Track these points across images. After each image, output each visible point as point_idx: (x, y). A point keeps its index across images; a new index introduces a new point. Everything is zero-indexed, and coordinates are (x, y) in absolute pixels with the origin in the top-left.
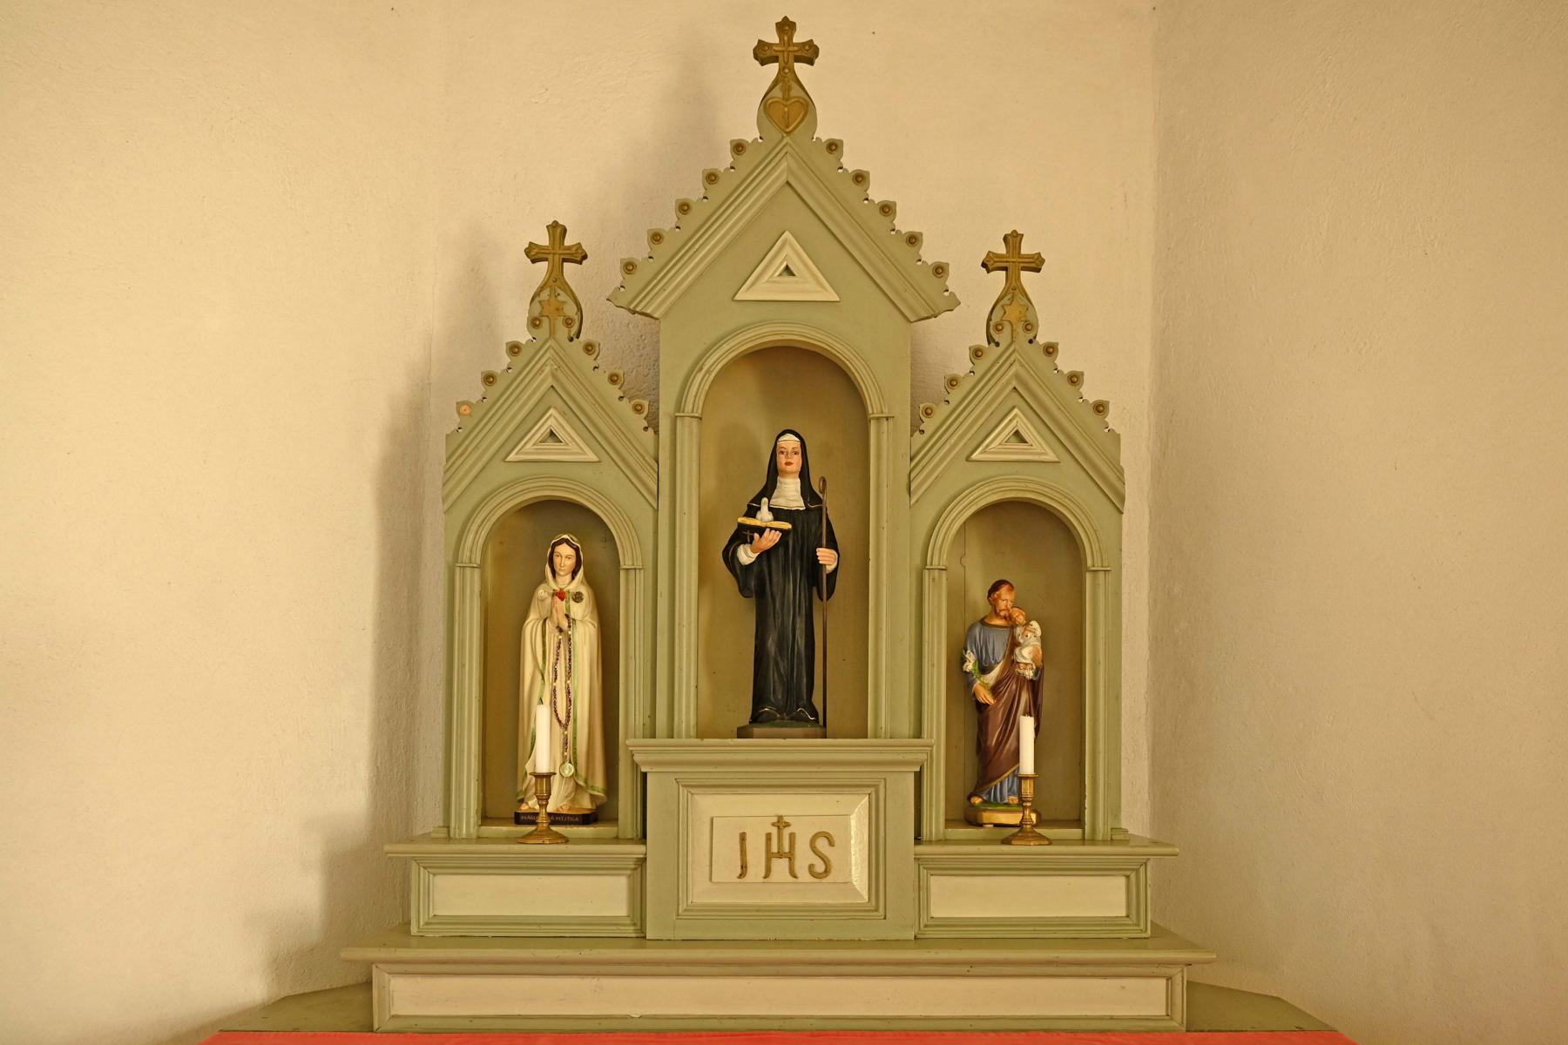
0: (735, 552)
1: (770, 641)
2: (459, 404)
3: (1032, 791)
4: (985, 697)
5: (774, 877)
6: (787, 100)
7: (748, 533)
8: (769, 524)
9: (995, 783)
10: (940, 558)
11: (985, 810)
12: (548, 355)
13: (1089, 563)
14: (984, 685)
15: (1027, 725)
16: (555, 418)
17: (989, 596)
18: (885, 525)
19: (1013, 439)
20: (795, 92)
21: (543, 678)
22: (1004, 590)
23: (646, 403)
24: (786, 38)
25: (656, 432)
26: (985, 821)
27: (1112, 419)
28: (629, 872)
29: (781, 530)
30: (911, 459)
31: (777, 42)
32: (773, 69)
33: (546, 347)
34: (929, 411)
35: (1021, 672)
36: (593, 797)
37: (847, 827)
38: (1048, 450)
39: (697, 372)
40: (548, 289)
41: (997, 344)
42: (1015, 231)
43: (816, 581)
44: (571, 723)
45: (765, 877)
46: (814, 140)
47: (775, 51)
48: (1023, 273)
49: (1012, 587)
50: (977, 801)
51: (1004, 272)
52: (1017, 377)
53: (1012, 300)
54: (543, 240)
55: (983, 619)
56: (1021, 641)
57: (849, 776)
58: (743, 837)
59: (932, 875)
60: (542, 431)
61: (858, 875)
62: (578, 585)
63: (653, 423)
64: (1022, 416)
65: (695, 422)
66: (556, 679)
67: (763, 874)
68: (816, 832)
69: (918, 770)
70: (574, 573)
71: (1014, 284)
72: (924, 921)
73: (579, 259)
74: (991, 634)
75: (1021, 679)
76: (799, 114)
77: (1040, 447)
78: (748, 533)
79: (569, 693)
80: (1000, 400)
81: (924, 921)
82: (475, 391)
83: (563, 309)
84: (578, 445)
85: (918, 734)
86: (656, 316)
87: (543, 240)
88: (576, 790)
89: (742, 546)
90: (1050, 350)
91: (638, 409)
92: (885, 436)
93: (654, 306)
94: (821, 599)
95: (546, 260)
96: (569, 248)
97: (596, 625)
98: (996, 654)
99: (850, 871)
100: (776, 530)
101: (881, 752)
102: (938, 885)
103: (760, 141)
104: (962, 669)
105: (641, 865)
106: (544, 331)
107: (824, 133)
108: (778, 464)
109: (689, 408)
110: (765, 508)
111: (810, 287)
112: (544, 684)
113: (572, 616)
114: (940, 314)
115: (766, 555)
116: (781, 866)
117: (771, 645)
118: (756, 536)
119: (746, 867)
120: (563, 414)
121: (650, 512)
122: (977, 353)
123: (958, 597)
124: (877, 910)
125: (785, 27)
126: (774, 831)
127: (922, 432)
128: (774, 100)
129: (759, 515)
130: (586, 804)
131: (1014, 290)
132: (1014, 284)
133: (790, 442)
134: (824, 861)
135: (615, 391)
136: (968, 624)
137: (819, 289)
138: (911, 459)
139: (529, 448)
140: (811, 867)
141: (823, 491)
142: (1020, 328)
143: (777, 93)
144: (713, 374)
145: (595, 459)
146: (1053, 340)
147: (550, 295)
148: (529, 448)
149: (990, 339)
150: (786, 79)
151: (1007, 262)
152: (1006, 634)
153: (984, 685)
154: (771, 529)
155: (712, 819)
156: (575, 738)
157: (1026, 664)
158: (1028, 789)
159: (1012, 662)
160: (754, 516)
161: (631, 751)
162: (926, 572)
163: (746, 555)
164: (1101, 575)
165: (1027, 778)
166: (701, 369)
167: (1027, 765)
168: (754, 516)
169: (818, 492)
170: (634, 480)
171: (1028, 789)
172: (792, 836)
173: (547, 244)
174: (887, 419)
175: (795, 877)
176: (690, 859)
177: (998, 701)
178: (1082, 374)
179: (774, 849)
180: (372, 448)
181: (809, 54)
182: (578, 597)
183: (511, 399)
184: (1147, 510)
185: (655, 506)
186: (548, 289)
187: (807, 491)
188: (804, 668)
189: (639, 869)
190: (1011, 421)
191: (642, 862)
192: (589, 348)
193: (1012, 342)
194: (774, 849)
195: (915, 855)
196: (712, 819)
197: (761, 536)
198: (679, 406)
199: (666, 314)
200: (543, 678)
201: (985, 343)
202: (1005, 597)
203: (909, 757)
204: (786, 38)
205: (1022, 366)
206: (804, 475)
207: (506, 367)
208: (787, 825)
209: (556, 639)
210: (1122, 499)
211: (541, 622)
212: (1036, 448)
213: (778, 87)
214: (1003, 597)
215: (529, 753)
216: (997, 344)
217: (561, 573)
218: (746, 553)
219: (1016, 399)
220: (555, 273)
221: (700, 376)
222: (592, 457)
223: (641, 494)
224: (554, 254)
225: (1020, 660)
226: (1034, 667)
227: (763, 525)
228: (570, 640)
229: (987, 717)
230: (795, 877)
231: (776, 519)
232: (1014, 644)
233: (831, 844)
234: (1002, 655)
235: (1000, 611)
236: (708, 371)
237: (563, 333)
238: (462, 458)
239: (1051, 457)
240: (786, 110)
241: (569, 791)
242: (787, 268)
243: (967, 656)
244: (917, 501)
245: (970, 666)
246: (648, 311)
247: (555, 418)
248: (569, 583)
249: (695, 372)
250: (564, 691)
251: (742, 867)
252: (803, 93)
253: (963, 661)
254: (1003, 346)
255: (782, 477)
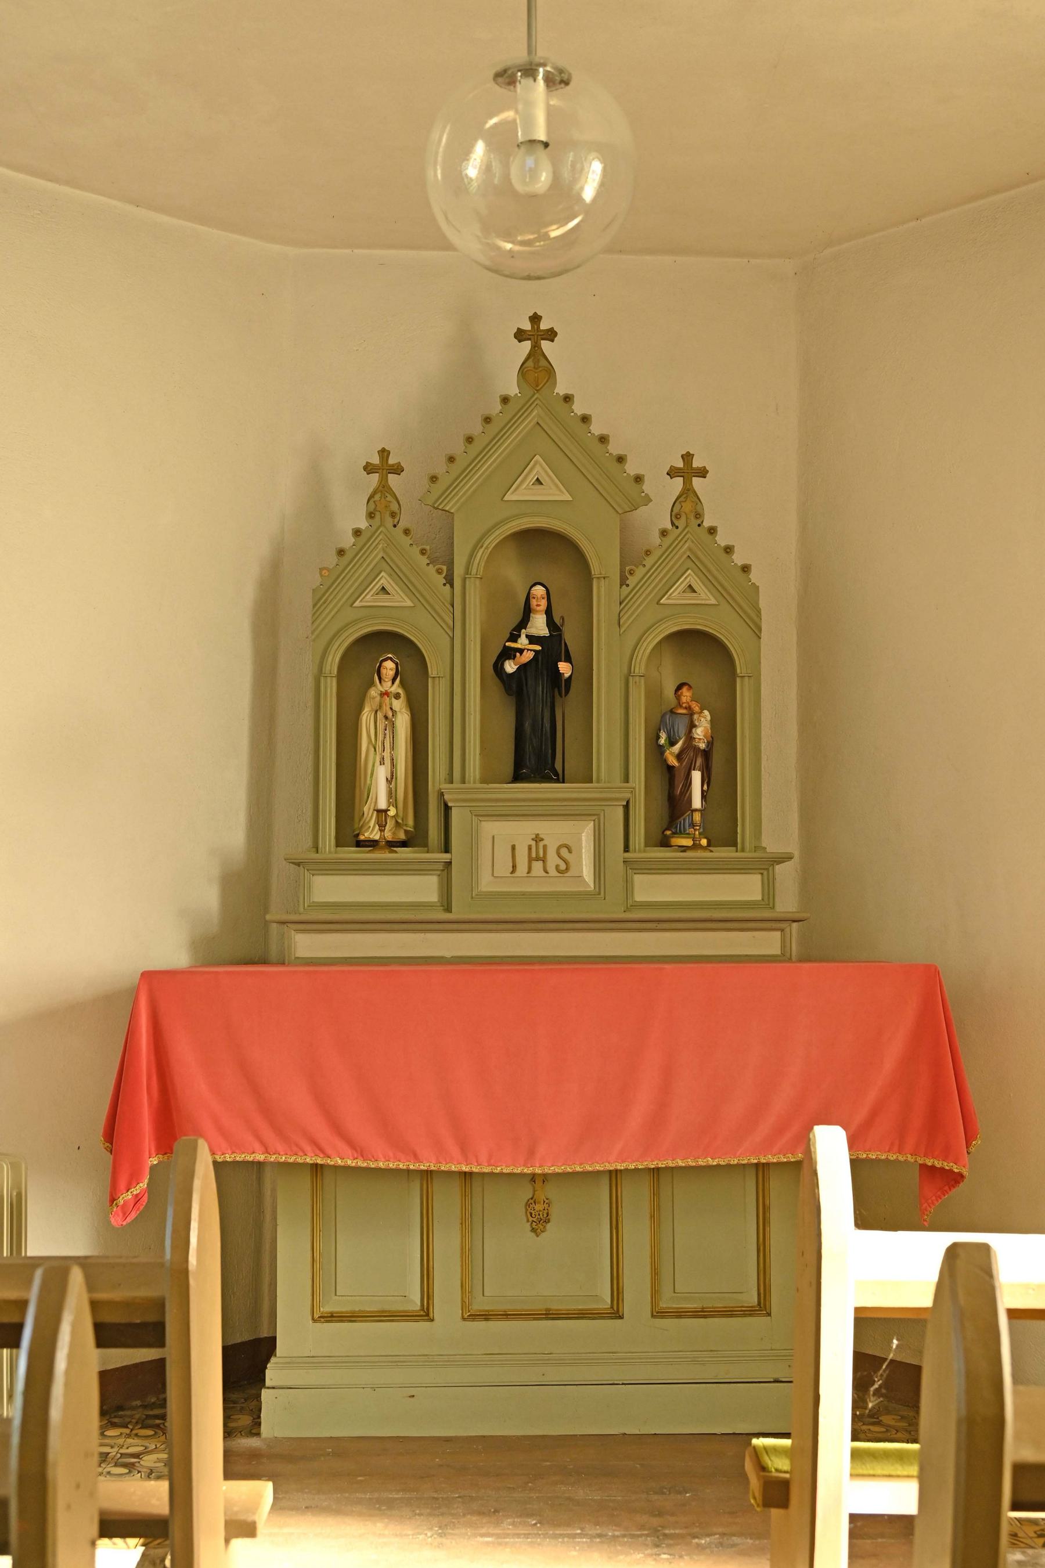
0: (503, 665)
1: (527, 724)
2: (321, 569)
3: (700, 819)
4: (673, 761)
5: (533, 873)
6: (537, 369)
7: (513, 652)
8: (527, 647)
9: (680, 820)
10: (639, 668)
11: (673, 837)
12: (381, 537)
13: (738, 671)
14: (672, 754)
15: (696, 776)
16: (386, 579)
17: (675, 694)
18: (603, 647)
19: (688, 590)
20: (543, 363)
21: (375, 750)
22: (685, 689)
23: (444, 568)
24: (536, 327)
25: (452, 586)
26: (673, 844)
27: (754, 576)
28: (439, 872)
29: (534, 651)
30: (620, 604)
31: (530, 329)
32: (527, 345)
33: (379, 532)
34: (632, 572)
35: (697, 744)
36: (406, 832)
37: (580, 840)
38: (711, 597)
39: (480, 548)
40: (380, 493)
41: (677, 527)
42: (688, 452)
43: (558, 685)
44: (394, 780)
45: (528, 873)
46: (555, 394)
47: (529, 335)
48: (694, 479)
49: (690, 687)
50: (668, 833)
51: (682, 478)
52: (690, 549)
53: (686, 498)
54: (376, 460)
55: (672, 709)
56: (697, 724)
57: (583, 808)
58: (513, 848)
59: (635, 874)
60: (377, 587)
61: (587, 873)
62: (396, 688)
63: (450, 581)
64: (693, 574)
65: (478, 582)
66: (384, 750)
67: (526, 871)
68: (560, 844)
69: (625, 803)
70: (394, 681)
71: (688, 487)
72: (630, 902)
73: (399, 473)
74: (677, 719)
75: (697, 749)
76: (545, 378)
77: (705, 595)
78: (513, 652)
79: (393, 760)
80: (673, 571)
81: (630, 902)
82: (332, 560)
83: (389, 506)
84: (402, 597)
85: (626, 779)
86: (452, 511)
87: (376, 460)
88: (396, 827)
89: (507, 662)
90: (712, 531)
91: (439, 572)
92: (603, 589)
93: (450, 505)
94: (561, 697)
95: (378, 473)
96: (393, 465)
97: (410, 715)
98: (679, 733)
99: (582, 869)
100: (531, 650)
101: (601, 792)
102: (639, 880)
103: (519, 395)
104: (657, 742)
105: (447, 868)
106: (377, 521)
107: (561, 389)
108: (531, 607)
109: (474, 571)
110: (523, 636)
111: (554, 492)
112: (376, 754)
113: (394, 708)
114: (638, 508)
115: (523, 668)
116: (538, 866)
117: (527, 725)
118: (518, 654)
119: (516, 866)
120: (390, 575)
121: (448, 640)
122: (664, 533)
123: (653, 694)
124: (762, 1307)
125: (535, 319)
126: (533, 843)
127: (628, 585)
128: (529, 369)
129: (519, 641)
130: (402, 836)
131: (688, 491)
132: (688, 487)
133: (539, 590)
134: (565, 862)
135: (407, 540)
136: (664, 712)
137: (558, 493)
138: (620, 604)
139: (369, 598)
140: (557, 867)
141: (562, 626)
142: (692, 517)
143: (530, 363)
144: (490, 549)
145: (412, 605)
146: (714, 525)
147: (381, 497)
148: (369, 598)
149: (673, 524)
150: (536, 352)
151: (683, 472)
152: (686, 720)
153: (672, 754)
154: (528, 650)
155: (493, 837)
156: (396, 791)
157: (700, 739)
158: (697, 817)
159: (690, 738)
160: (516, 641)
161: (443, 792)
162: (631, 678)
163: (510, 667)
164: (746, 679)
165: (696, 810)
166: (482, 547)
167: (697, 802)
168: (516, 641)
169: (559, 625)
170: (437, 618)
171: (697, 817)
172: (545, 847)
173: (378, 463)
174: (604, 578)
175: (547, 873)
176: (479, 862)
177: (681, 764)
178: (734, 546)
179: (534, 855)
180: (249, 594)
181: (551, 335)
182: (397, 696)
183: (357, 566)
184: (795, 632)
185: (451, 635)
186: (380, 493)
187: (551, 623)
188: (549, 742)
189: (446, 870)
190: (686, 578)
191: (449, 864)
192: (407, 532)
193: (686, 527)
194: (534, 855)
195: (624, 859)
196: (493, 837)
197: (521, 655)
198: (467, 571)
199: (458, 510)
200: (375, 750)
201: (669, 526)
202: (686, 695)
203: (618, 795)
204: (536, 327)
205: (693, 542)
206: (549, 612)
207: (351, 545)
208: (542, 840)
209: (383, 723)
210: (760, 630)
211: (374, 712)
212: (703, 595)
213: (531, 360)
214: (684, 694)
215: (365, 801)
216: (677, 527)
217: (387, 680)
218: (510, 666)
219: (689, 564)
220: (383, 483)
221: (481, 550)
222: (409, 603)
223: (441, 626)
224: (383, 469)
225: (696, 736)
226: (706, 741)
227: (523, 647)
228: (393, 724)
229: (674, 776)
230: (547, 873)
231: (530, 643)
232: (692, 726)
233: (570, 851)
234: (684, 732)
235: (683, 703)
236: (487, 548)
237: (389, 522)
238: (325, 605)
239: (713, 601)
240: (536, 375)
241: (391, 826)
242: (538, 479)
243: (660, 734)
244: (624, 631)
245: (662, 741)
246: (447, 509)
247: (386, 579)
248: (391, 687)
249: (478, 548)
250: (389, 758)
251: (513, 867)
252: (547, 363)
253: (658, 737)
254: (680, 529)
255: (534, 614)
